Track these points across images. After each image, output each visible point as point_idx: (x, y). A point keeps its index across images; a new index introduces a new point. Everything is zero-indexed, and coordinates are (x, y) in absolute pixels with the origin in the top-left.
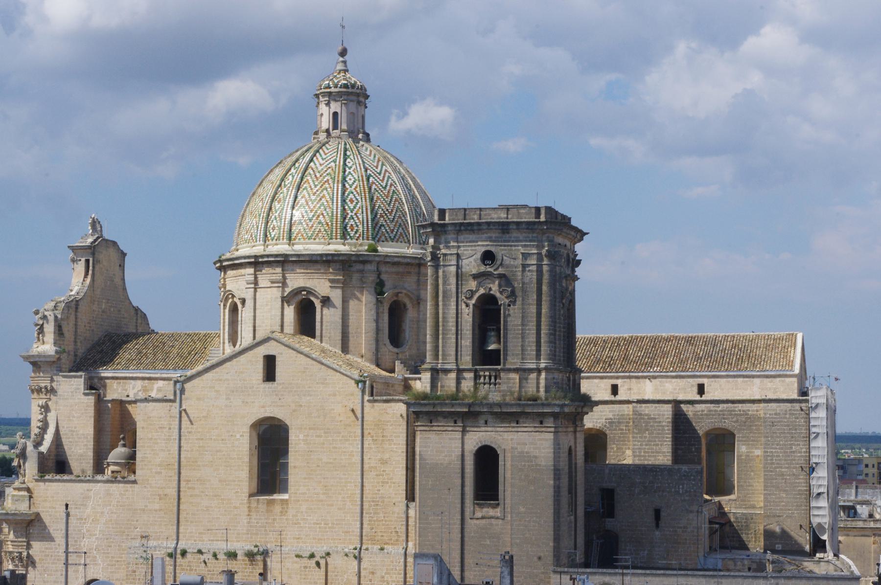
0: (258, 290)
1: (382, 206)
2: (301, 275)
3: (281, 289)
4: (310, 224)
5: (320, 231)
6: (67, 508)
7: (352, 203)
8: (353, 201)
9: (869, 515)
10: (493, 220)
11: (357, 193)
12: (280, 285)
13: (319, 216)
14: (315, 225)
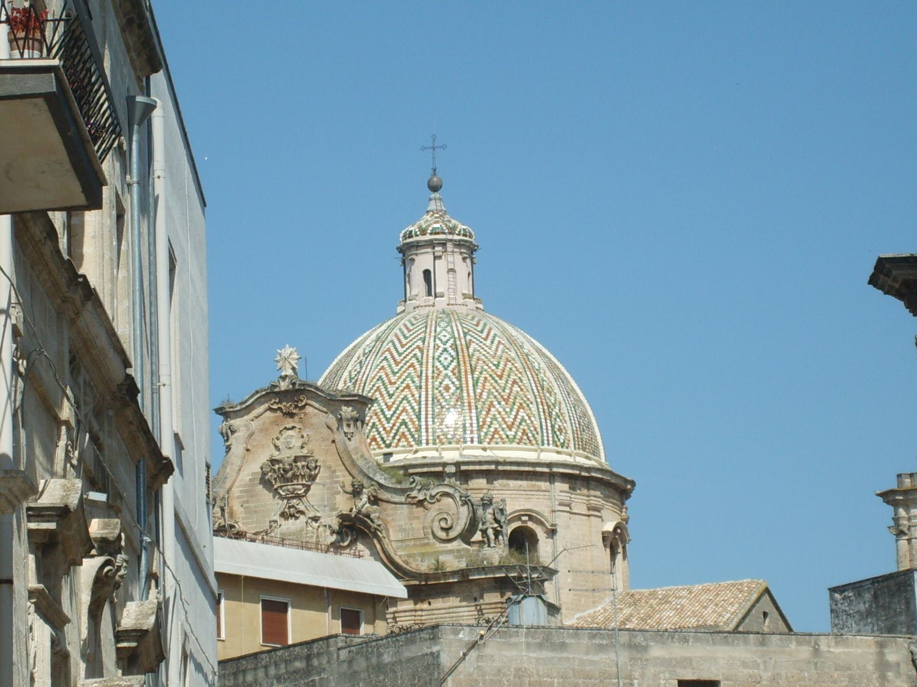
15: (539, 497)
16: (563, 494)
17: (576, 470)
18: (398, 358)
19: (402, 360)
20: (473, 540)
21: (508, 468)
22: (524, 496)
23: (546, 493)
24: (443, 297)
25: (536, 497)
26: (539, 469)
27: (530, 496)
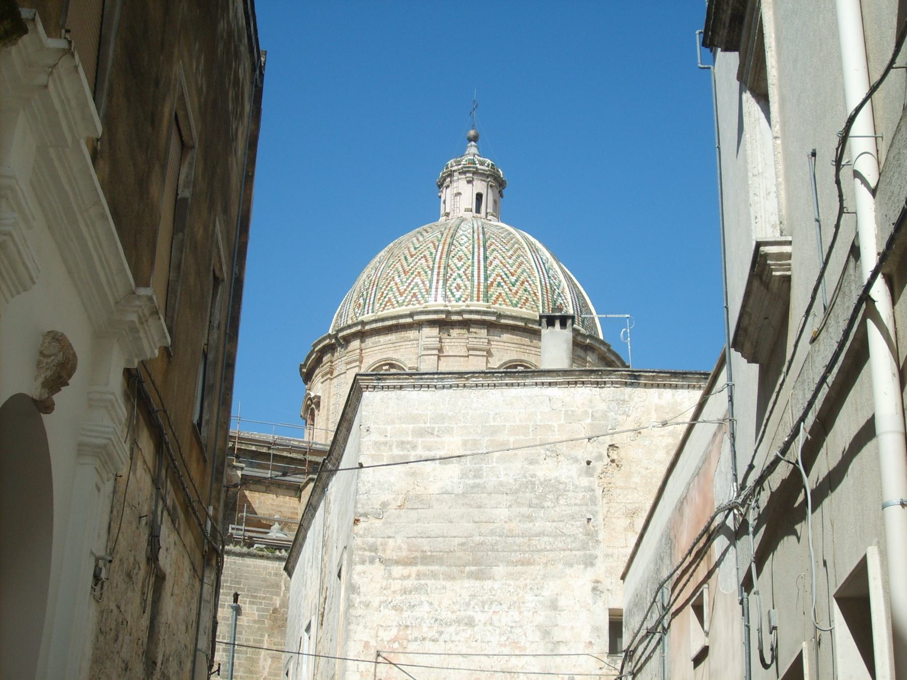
0: (442, 358)
1: (511, 296)
2: (514, 345)
3: (485, 358)
4: (514, 289)
5: (527, 299)
6: (236, 600)
7: (458, 285)
8: (460, 288)
9: (812, 153)
10: (224, 613)
11: (467, 278)
12: (485, 353)
13: (523, 283)
14: (520, 292)
15: (406, 346)
16: (429, 339)
17: (522, 322)
18: (407, 269)
19: (410, 270)
20: (851, 256)
21: (374, 326)
22: (392, 349)
23: (415, 342)
24: (659, 398)
25: (404, 347)
26: (402, 321)
27: (398, 348)
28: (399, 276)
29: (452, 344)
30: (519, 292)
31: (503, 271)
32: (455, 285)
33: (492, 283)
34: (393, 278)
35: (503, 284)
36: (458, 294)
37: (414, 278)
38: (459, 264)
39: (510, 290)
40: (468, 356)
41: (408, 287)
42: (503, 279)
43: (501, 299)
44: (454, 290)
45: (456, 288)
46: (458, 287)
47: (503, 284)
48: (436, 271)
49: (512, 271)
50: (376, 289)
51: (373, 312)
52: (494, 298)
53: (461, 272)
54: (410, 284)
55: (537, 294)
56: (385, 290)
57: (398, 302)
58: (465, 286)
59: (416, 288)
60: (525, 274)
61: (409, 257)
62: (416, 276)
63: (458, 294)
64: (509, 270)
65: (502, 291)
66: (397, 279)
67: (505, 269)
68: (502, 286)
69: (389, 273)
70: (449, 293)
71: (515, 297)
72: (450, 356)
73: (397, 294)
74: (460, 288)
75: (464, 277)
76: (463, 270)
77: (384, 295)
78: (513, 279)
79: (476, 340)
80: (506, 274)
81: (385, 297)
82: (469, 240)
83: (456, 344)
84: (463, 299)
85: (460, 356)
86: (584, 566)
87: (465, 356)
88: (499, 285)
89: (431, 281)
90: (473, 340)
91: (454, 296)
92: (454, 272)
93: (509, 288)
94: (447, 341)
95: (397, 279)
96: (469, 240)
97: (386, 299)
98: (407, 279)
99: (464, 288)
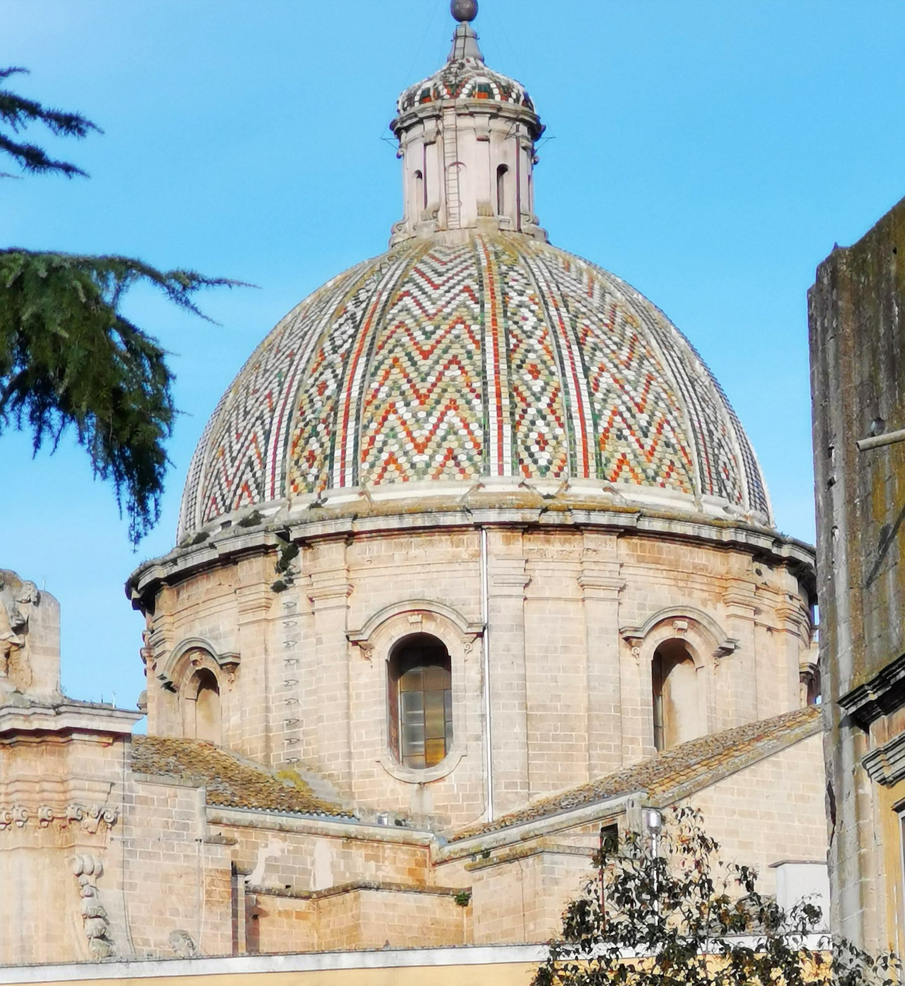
4: (648, 442)
7: (541, 435)
14: (658, 448)
28: (407, 404)
29: (550, 573)
30: (657, 448)
31: (624, 403)
32: (534, 436)
33: (607, 430)
34: (392, 405)
35: (626, 432)
36: (543, 458)
37: (443, 414)
38: (537, 386)
39: (642, 446)
40: (583, 600)
41: (432, 432)
42: (624, 420)
43: (625, 468)
44: (535, 448)
45: (538, 443)
46: (542, 442)
47: (626, 432)
48: (493, 401)
49: (638, 400)
50: (357, 431)
51: (356, 483)
52: (613, 465)
53: (543, 404)
54: (436, 427)
55: (688, 450)
56: (377, 432)
57: (413, 466)
58: (555, 438)
59: (451, 437)
60: (661, 403)
61: (418, 357)
62: (448, 408)
63: (543, 458)
64: (632, 399)
65: (627, 450)
66: (400, 405)
67: (626, 398)
68: (626, 438)
69: (377, 391)
70: (524, 455)
71: (650, 461)
72: (548, 599)
73: (410, 446)
74: (546, 443)
75: (551, 418)
76: (545, 400)
77: (378, 444)
78: (643, 419)
79: (597, 568)
80: (629, 410)
81: (380, 451)
82: (541, 320)
83: (557, 574)
84: (554, 469)
85: (566, 600)
86: (54, 265)
87: (577, 600)
88: (620, 437)
89: (485, 426)
90: (593, 566)
91: (535, 462)
92: (529, 405)
93: (638, 441)
94: (539, 571)
95: (400, 405)
96: (541, 320)
97: (385, 456)
98: (429, 414)
99: (553, 442)
